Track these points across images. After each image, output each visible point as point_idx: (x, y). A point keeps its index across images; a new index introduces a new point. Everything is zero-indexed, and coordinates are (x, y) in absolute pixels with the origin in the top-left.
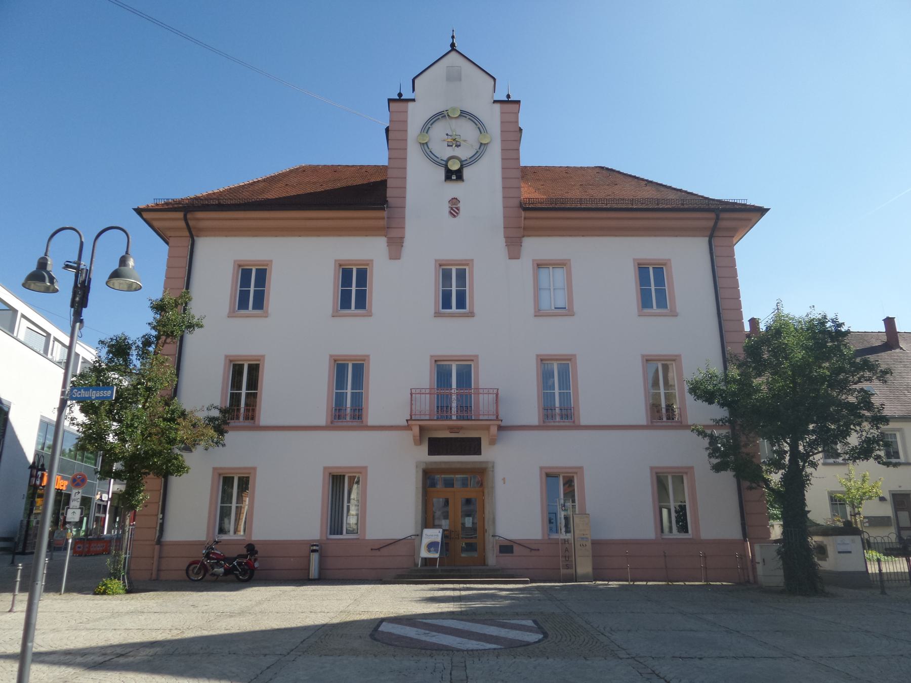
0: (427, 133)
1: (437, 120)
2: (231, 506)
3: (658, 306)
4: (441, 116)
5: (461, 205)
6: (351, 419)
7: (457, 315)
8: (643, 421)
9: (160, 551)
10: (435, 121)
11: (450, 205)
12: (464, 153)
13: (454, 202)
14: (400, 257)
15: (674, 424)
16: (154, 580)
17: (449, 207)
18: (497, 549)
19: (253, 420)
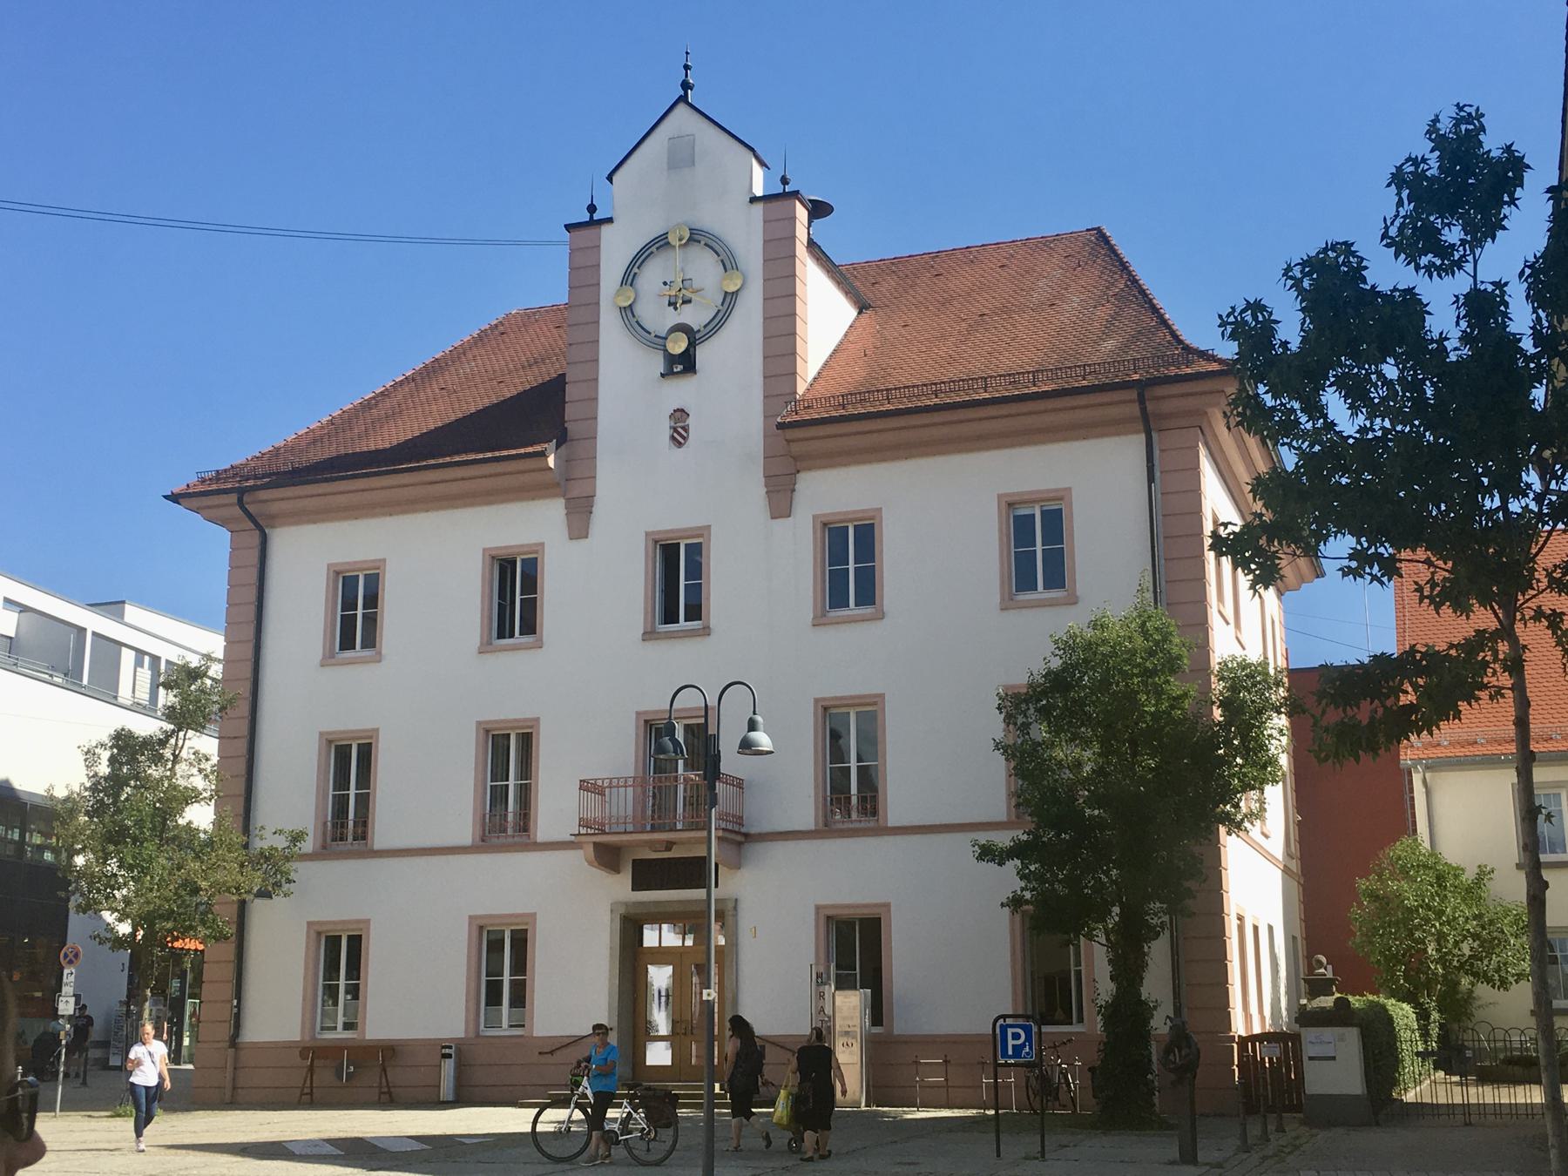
0: (631, 285)
1: (649, 255)
2: (338, 984)
3: (1048, 586)
4: (661, 243)
5: (691, 421)
6: (515, 831)
7: (681, 635)
9: (236, 1059)
10: (643, 261)
11: (673, 424)
12: (694, 316)
13: (680, 414)
14: (588, 534)
15: (851, 826)
16: (227, 1104)
17: (670, 428)
19: (365, 840)
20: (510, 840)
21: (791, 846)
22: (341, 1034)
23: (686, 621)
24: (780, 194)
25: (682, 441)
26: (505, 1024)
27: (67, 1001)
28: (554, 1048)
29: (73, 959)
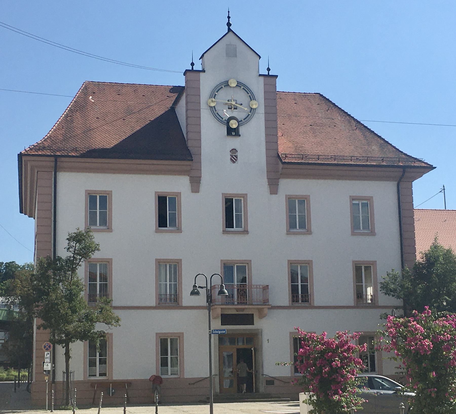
2: (167, 357)
5: (239, 154)
8: (352, 304)
12: (240, 115)
17: (230, 155)
18: (264, 384)
20: (300, 305)
21: (280, 311)
22: (98, 378)
23: (236, 228)
24: (267, 75)
25: (235, 161)
26: (169, 373)
27: (47, 365)
28: (194, 382)
29: (49, 348)
